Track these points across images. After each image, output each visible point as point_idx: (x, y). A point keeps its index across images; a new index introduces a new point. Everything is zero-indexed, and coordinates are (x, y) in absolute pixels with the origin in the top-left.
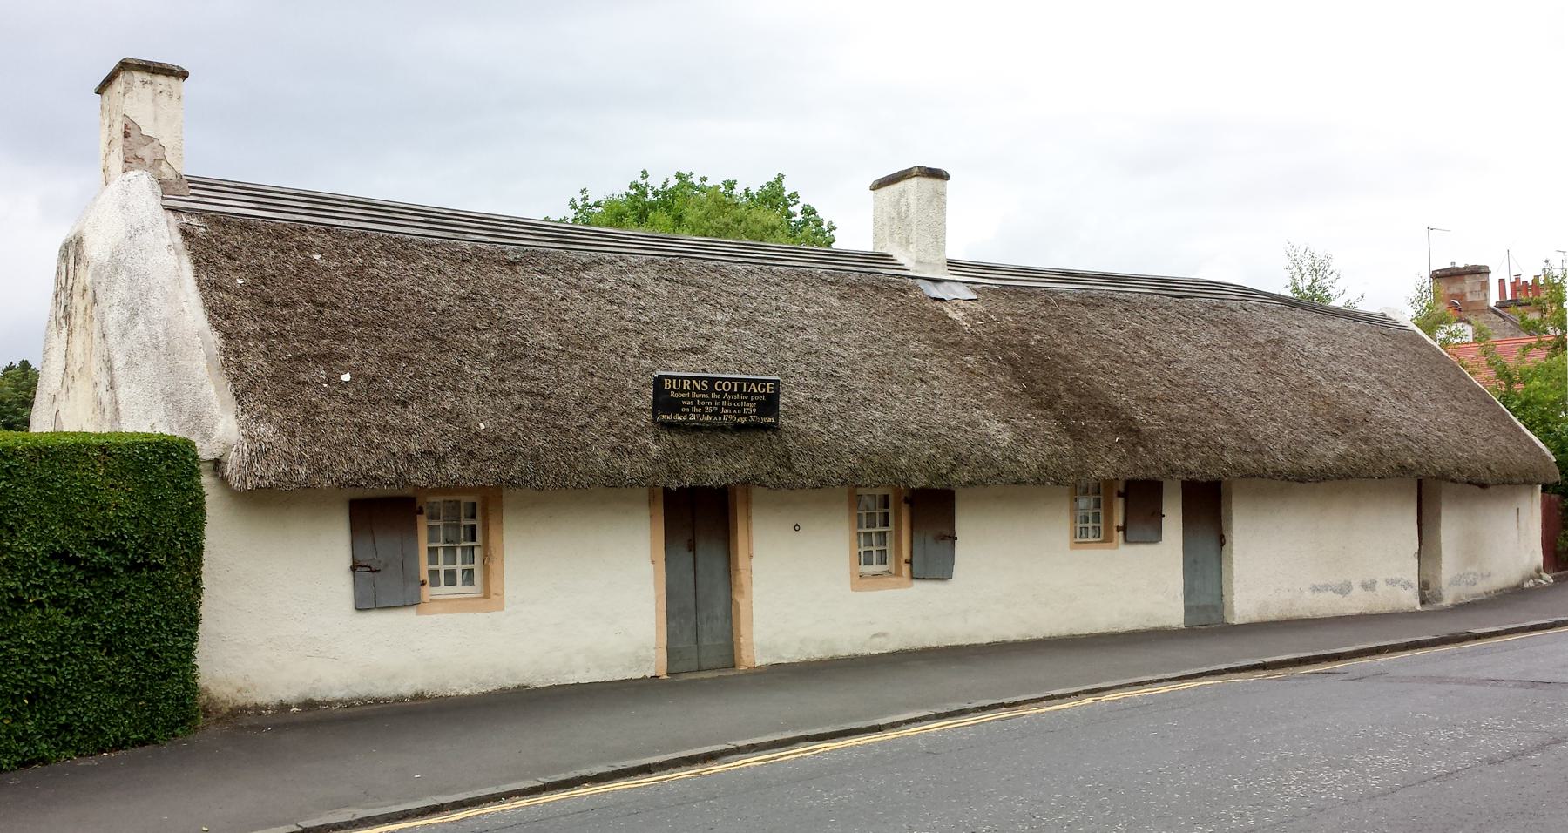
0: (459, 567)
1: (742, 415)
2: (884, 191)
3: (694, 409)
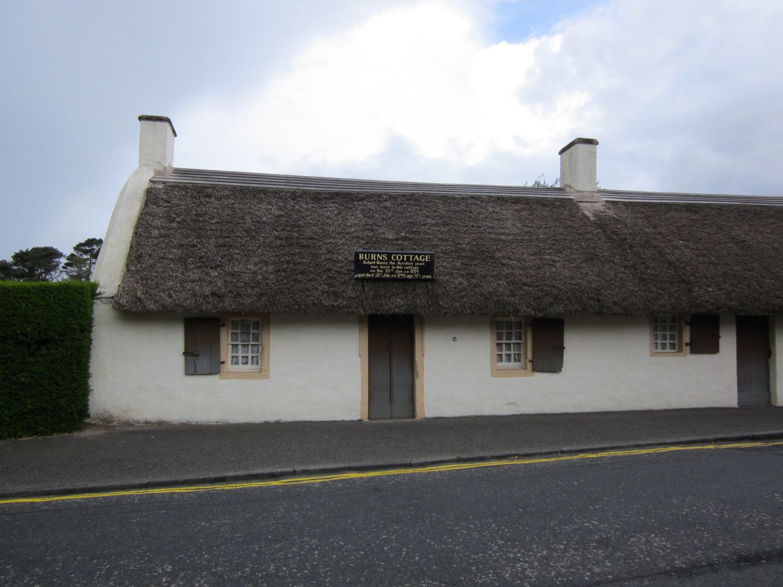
0: (250, 355)
1: (410, 274)
2: (564, 153)
3: (378, 270)
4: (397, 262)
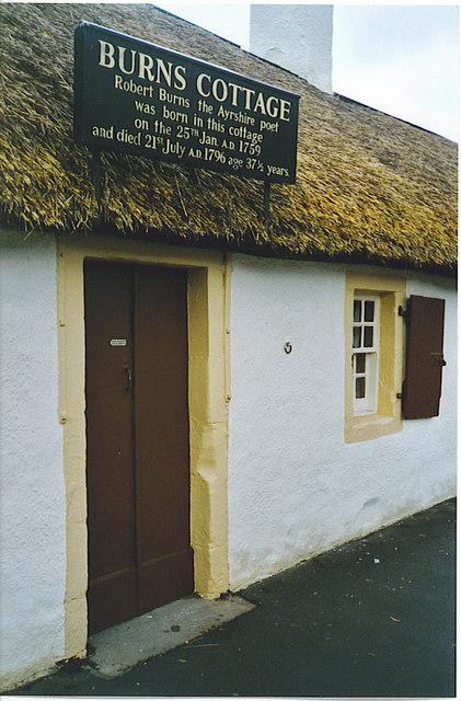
4: (216, 105)
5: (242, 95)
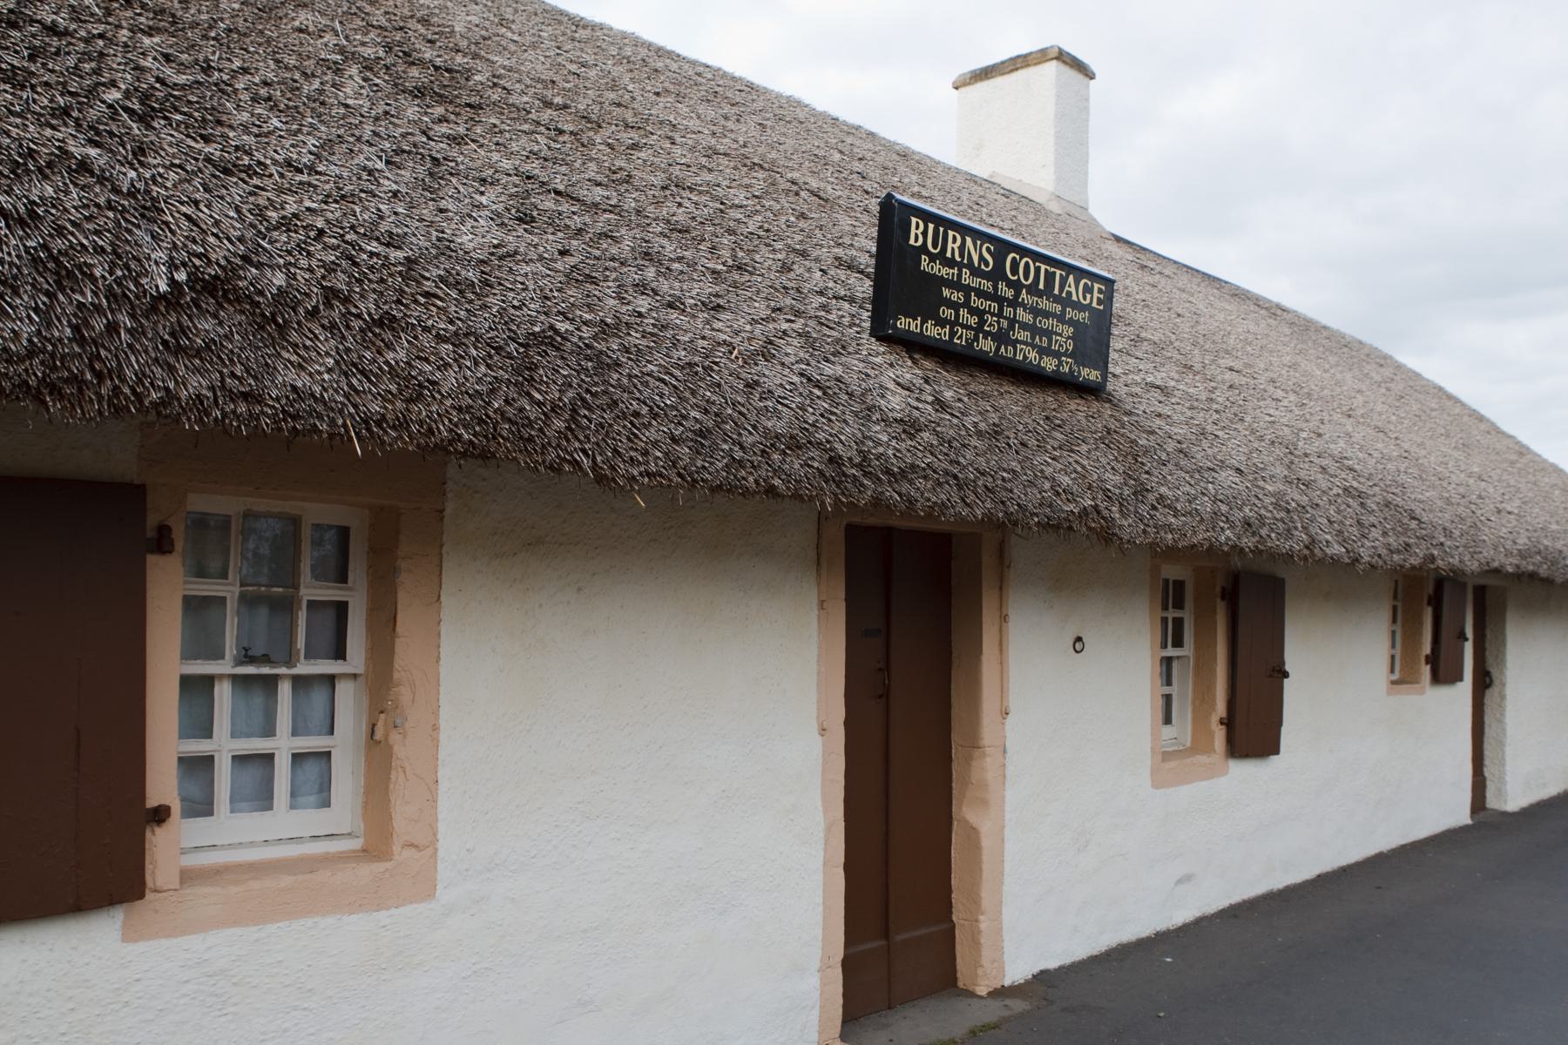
0: (283, 745)
5: (1050, 277)
